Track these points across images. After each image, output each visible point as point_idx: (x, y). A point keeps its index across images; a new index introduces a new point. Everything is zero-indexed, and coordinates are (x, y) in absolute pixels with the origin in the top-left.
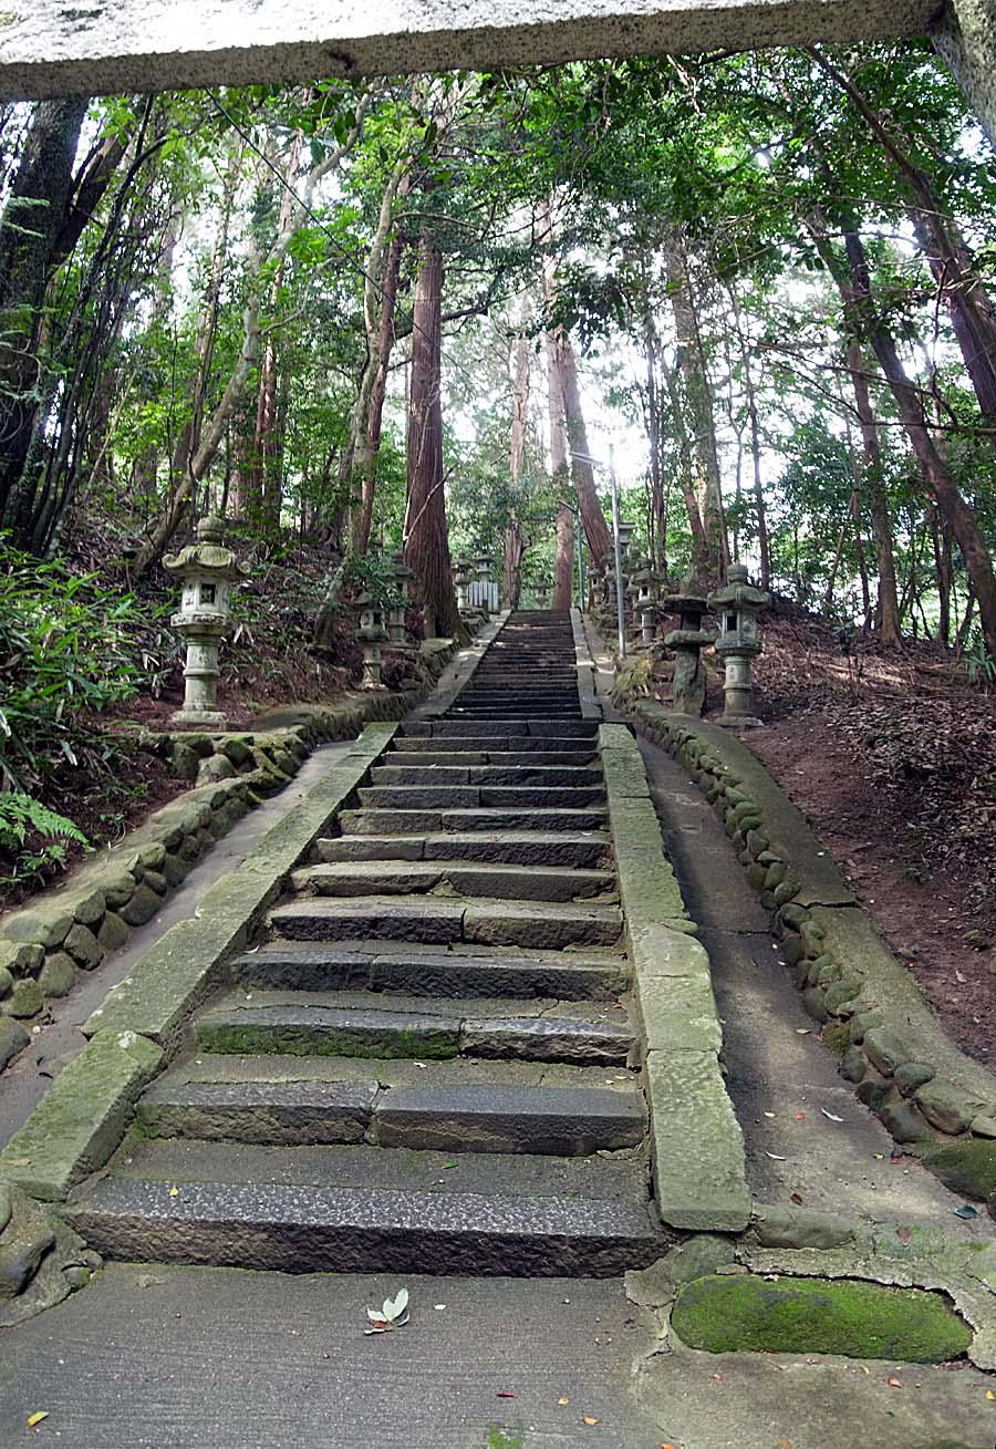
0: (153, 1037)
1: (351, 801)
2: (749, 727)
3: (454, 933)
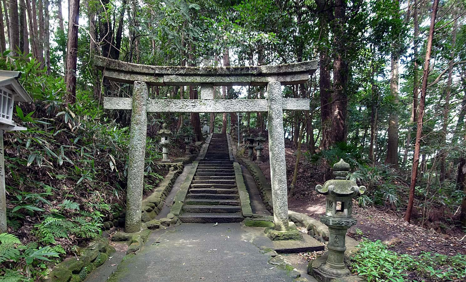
0: (182, 202)
1: (195, 175)
2: (260, 163)
3: (216, 192)
